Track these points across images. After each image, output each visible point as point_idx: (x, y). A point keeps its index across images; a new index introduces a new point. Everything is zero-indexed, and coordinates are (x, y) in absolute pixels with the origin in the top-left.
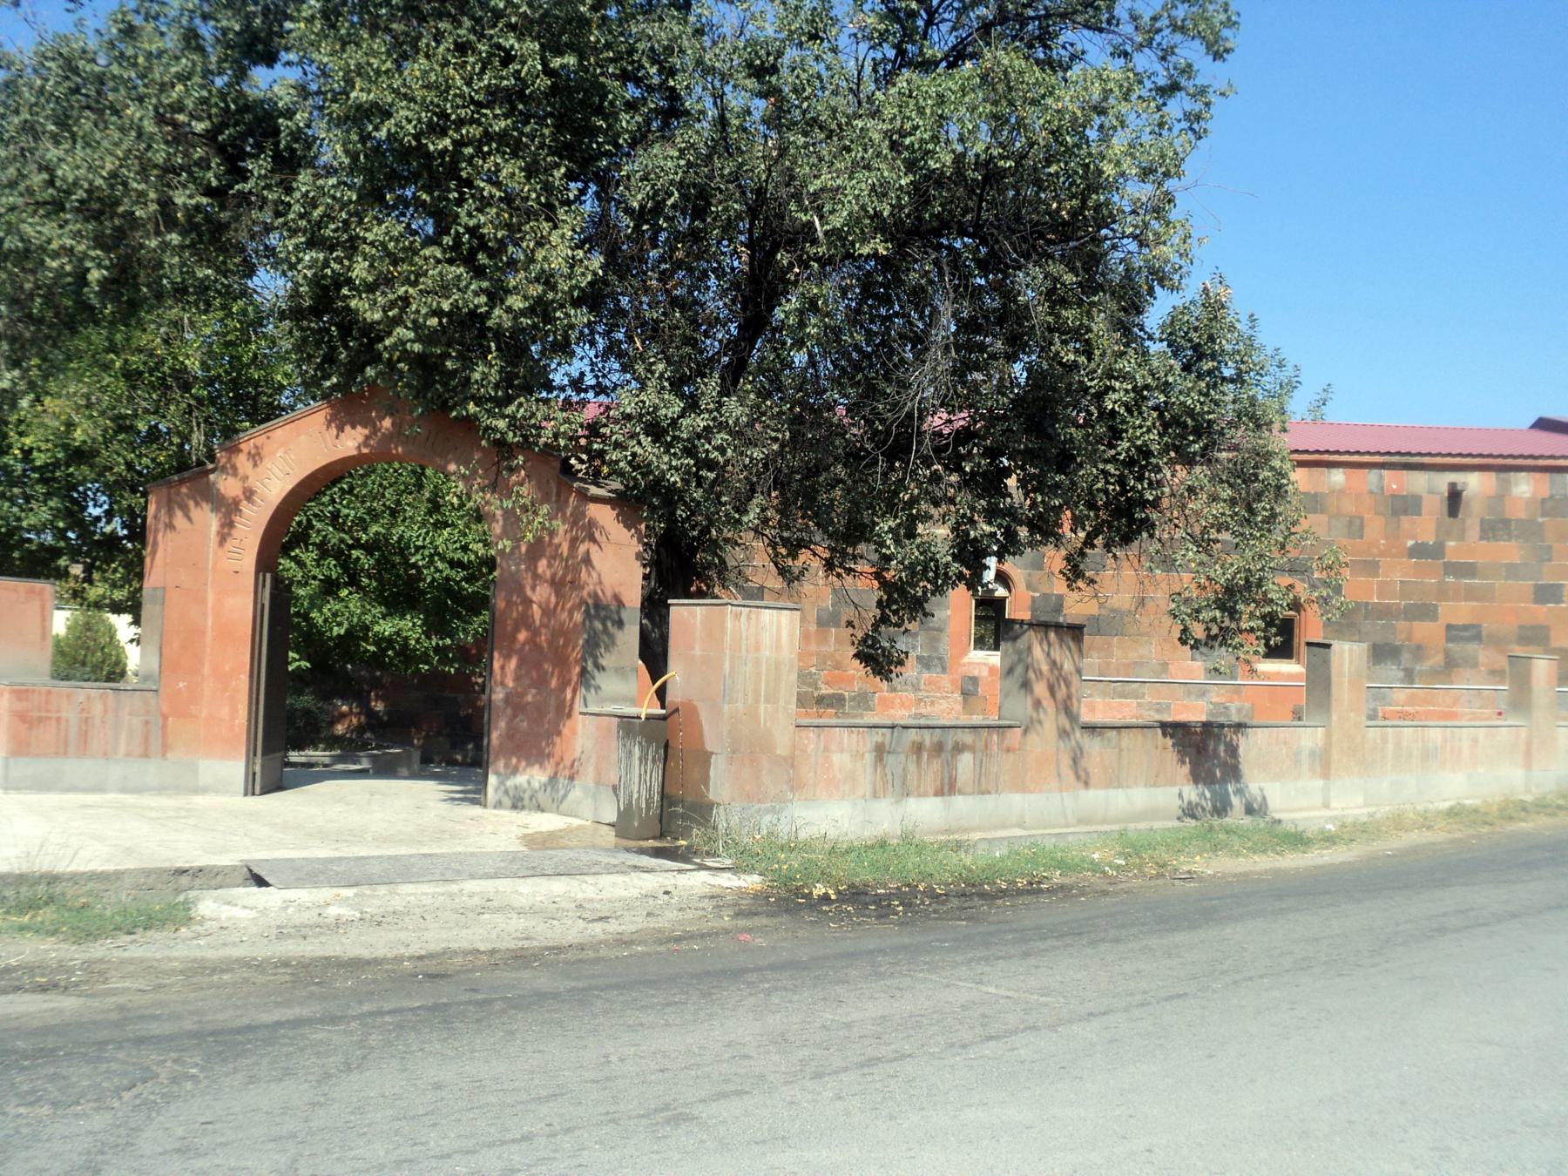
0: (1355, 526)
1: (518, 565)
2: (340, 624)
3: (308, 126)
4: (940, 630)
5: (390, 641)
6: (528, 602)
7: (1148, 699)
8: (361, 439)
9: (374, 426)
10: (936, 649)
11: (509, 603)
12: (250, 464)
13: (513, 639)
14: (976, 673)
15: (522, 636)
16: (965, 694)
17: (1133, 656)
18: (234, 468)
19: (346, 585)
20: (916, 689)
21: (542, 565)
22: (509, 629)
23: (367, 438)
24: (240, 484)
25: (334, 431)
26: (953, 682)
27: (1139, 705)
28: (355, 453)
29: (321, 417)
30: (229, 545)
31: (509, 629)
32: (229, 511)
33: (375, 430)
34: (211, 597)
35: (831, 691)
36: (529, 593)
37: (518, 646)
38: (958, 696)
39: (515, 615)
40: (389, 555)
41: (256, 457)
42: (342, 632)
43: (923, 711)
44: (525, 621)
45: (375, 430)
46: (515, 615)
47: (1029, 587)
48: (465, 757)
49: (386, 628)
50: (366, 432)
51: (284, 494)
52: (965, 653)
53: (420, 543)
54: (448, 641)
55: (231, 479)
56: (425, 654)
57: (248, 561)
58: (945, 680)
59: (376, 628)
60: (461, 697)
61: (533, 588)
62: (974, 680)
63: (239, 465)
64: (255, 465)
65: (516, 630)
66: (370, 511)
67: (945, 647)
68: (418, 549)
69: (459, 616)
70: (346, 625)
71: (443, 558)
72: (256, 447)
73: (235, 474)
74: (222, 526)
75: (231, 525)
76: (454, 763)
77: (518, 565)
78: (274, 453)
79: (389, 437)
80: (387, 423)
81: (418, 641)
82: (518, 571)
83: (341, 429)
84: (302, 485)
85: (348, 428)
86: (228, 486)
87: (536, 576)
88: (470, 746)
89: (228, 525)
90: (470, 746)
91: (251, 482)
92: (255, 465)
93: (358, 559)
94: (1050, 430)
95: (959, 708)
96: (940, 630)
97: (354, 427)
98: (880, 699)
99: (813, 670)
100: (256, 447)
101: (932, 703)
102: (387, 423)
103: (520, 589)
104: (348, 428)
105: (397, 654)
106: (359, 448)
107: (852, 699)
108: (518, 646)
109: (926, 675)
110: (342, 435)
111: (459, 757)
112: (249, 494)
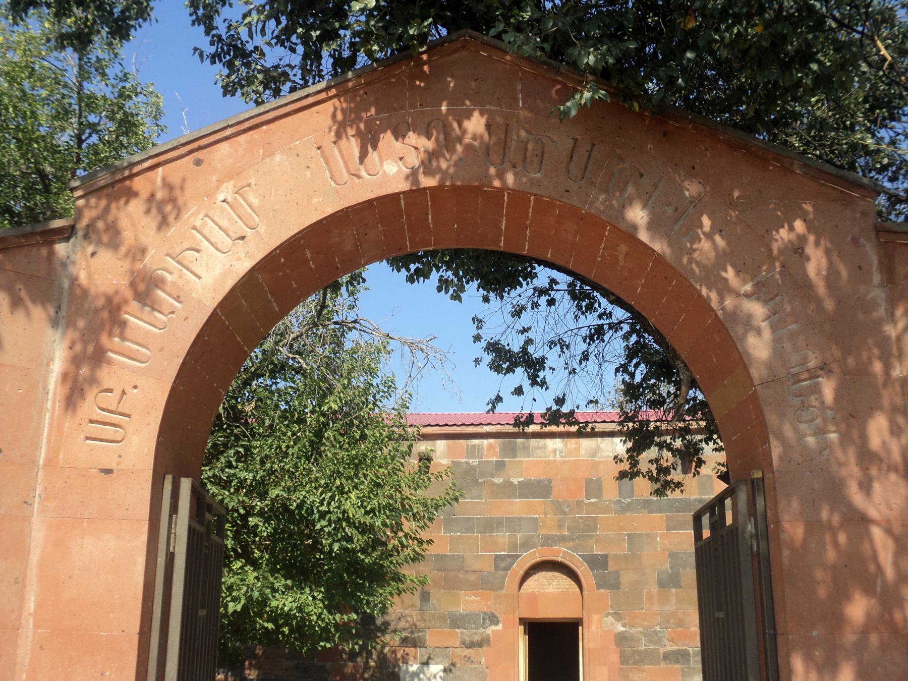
0: (274, 590)
1: (820, 432)
2: (234, 600)
5: (287, 616)
6: (859, 522)
8: (414, 160)
9: (446, 129)
11: (814, 526)
12: (149, 223)
13: (836, 620)
15: (858, 609)
18: (114, 230)
19: (238, 556)
21: (878, 429)
22: (822, 592)
23: (432, 155)
24: (126, 264)
25: (353, 146)
28: (403, 186)
29: (322, 118)
30: (89, 407)
31: (822, 592)
32: (94, 326)
33: (448, 142)
34: (38, 534)
35: (675, 648)
36: (857, 498)
37: (850, 638)
39: (831, 555)
40: (293, 522)
41: (166, 208)
42: (239, 608)
44: (857, 571)
45: (448, 142)
46: (831, 555)
49: (285, 602)
50: (430, 145)
51: (230, 284)
53: (324, 508)
55: (105, 257)
56: (326, 630)
57: (138, 444)
59: (274, 603)
60: (328, 665)
61: (866, 486)
63: (124, 223)
64: (163, 223)
65: (840, 595)
66: (272, 472)
68: (323, 515)
69: (361, 588)
70: (243, 601)
71: (351, 524)
72: (168, 185)
73: (114, 244)
74: (76, 361)
75: (99, 357)
77: (820, 432)
78: (211, 194)
79: (481, 154)
80: (476, 124)
81: (319, 617)
82: (825, 446)
83: (369, 141)
84: (268, 265)
85: (387, 138)
86: (95, 269)
87: (866, 457)
89: (89, 359)
91: (153, 260)
92: (163, 223)
93: (256, 525)
97: (399, 135)
99: (658, 628)
100: (168, 185)
102: (476, 124)
103: (834, 490)
104: (387, 138)
105: (292, 631)
106: (414, 174)
108: (850, 638)
110: (373, 156)
112: (145, 288)
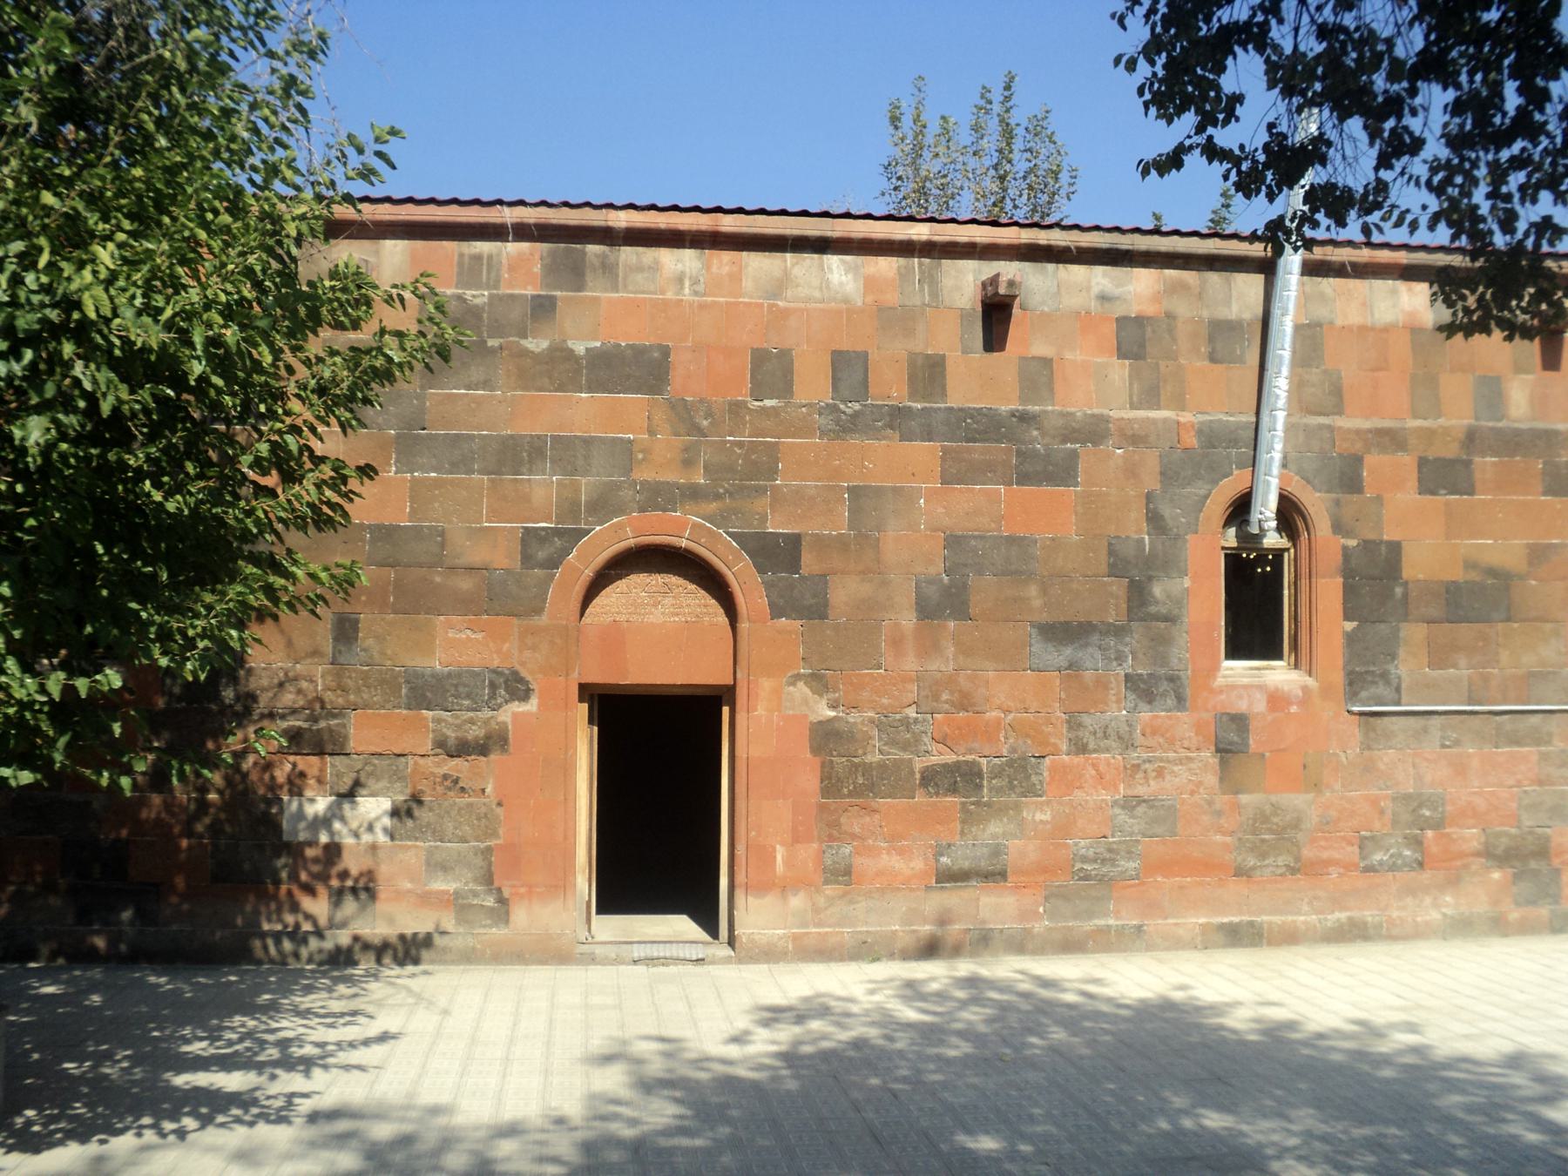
3: (299, 241)
4: (1170, 619)
7: (1558, 745)
10: (1162, 660)
14: (1242, 706)
16: (1225, 751)
17: (1529, 660)
20: (1127, 744)
26: (1199, 727)
27: (1544, 757)
35: (950, 758)
38: (1208, 756)
43: (1141, 790)
47: (1338, 528)
48: (113, 943)
52: (1215, 668)
54: (113, 678)
58: (1183, 723)
62: (1240, 721)
67: (1182, 654)
76: (89, 957)
88: (126, 915)
90: (126, 915)
94: (94, 101)
95: (1211, 779)
96: (1170, 619)
98: (1053, 769)
99: (911, 712)
101: (1160, 773)
107: (997, 773)
109: (1145, 715)
111: (100, 942)
